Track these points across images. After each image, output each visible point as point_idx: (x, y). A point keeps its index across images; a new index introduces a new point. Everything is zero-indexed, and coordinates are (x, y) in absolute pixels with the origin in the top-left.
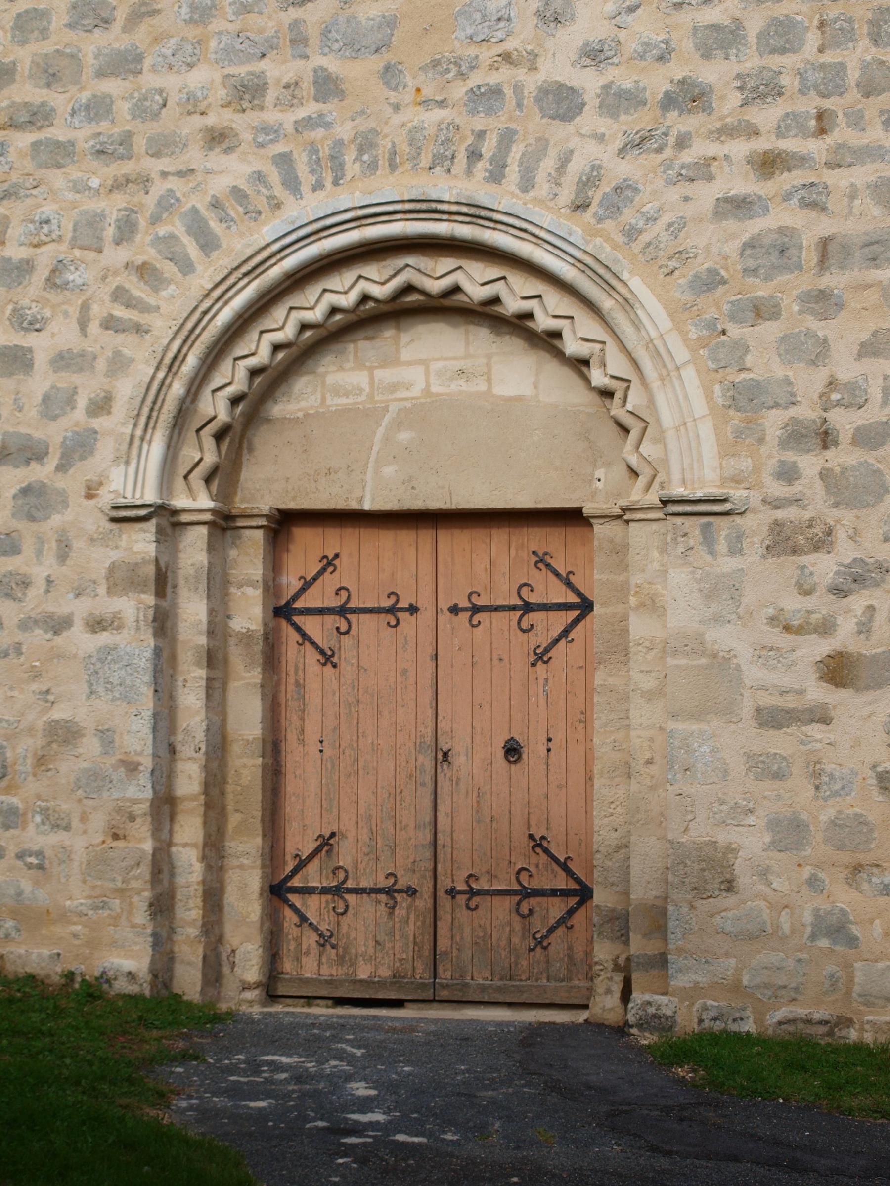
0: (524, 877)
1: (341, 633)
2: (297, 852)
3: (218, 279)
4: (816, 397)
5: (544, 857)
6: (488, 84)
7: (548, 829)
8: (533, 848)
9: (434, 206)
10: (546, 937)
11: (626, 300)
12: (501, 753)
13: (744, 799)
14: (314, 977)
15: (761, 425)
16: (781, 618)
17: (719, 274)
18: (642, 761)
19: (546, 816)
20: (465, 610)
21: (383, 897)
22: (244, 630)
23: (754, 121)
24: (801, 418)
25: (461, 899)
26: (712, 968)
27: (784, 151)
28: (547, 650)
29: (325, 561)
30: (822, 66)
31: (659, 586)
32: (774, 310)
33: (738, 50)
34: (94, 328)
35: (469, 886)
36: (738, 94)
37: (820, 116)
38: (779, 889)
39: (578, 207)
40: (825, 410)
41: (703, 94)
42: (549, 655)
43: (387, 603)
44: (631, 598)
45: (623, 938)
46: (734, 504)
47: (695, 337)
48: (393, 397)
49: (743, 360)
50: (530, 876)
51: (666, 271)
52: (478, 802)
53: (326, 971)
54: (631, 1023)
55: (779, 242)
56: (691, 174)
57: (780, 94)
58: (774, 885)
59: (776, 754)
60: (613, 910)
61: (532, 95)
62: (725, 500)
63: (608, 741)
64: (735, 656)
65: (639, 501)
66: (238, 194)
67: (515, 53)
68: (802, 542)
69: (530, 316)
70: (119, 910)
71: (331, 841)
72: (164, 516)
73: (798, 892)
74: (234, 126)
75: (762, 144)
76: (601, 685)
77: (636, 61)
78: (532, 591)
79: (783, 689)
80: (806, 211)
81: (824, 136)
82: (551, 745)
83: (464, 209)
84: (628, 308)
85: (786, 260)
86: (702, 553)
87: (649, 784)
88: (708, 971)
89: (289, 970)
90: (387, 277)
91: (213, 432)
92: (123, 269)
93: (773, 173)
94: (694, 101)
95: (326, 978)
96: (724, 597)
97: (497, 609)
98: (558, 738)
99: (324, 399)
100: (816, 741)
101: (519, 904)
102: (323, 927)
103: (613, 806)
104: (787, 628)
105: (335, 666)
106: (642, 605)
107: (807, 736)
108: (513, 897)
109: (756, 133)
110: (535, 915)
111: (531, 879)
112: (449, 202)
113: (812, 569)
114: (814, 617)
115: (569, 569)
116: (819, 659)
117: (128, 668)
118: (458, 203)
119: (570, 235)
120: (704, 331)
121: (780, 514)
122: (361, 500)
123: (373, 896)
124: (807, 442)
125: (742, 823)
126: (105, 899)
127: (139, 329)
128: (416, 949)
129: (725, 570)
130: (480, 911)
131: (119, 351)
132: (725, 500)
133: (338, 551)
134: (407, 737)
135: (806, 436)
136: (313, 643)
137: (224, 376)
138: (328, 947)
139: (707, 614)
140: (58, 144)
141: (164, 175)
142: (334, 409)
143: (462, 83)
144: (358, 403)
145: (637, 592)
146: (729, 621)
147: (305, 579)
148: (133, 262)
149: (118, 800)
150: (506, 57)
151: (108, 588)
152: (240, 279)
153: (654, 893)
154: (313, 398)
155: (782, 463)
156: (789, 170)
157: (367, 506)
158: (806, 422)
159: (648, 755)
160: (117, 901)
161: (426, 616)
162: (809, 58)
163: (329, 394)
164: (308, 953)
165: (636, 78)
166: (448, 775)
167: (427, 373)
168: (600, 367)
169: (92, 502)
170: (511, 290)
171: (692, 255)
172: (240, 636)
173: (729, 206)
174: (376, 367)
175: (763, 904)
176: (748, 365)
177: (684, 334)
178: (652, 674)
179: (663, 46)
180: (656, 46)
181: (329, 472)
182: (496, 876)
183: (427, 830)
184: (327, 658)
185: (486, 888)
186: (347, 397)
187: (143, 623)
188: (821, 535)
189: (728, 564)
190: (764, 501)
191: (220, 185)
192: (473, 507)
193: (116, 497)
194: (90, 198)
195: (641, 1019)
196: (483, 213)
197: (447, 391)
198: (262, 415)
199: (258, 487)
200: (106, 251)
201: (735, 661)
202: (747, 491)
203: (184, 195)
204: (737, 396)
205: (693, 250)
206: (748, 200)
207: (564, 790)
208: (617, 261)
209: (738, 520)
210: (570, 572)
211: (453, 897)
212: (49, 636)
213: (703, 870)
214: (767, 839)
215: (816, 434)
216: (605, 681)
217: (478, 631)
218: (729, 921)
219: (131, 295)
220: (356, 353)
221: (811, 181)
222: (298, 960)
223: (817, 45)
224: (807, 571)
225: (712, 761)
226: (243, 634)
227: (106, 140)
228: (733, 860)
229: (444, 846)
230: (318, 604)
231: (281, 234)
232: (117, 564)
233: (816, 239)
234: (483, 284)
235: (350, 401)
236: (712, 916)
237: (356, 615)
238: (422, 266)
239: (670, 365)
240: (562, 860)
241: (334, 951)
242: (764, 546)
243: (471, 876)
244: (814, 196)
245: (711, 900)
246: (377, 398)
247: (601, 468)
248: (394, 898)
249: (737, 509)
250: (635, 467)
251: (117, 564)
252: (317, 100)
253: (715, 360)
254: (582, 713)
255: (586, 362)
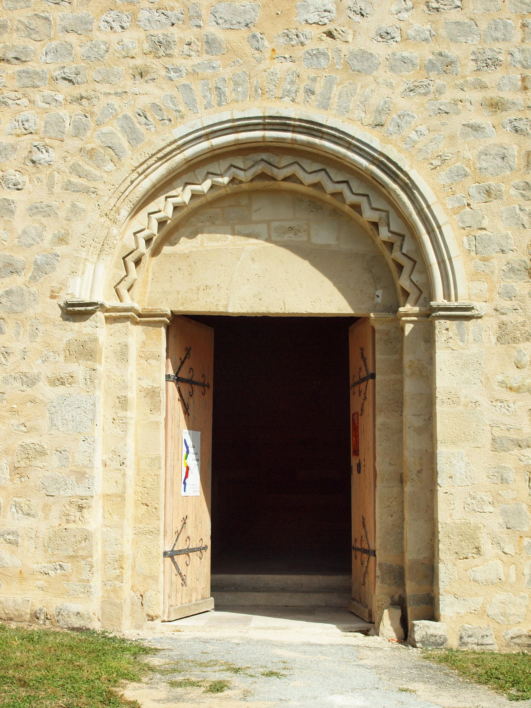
3: (142, 160)
22: (150, 387)
33: (473, 38)
34: (57, 189)
36: (473, 63)
70: (70, 571)
91: (134, 259)
94: (447, 66)
119: (372, 142)
122: (226, 306)
153: (423, 555)
160: (70, 565)
167: (269, 228)
177: (444, 205)
180: (423, 33)
191: (143, 102)
195: (423, 637)
238: (272, 160)
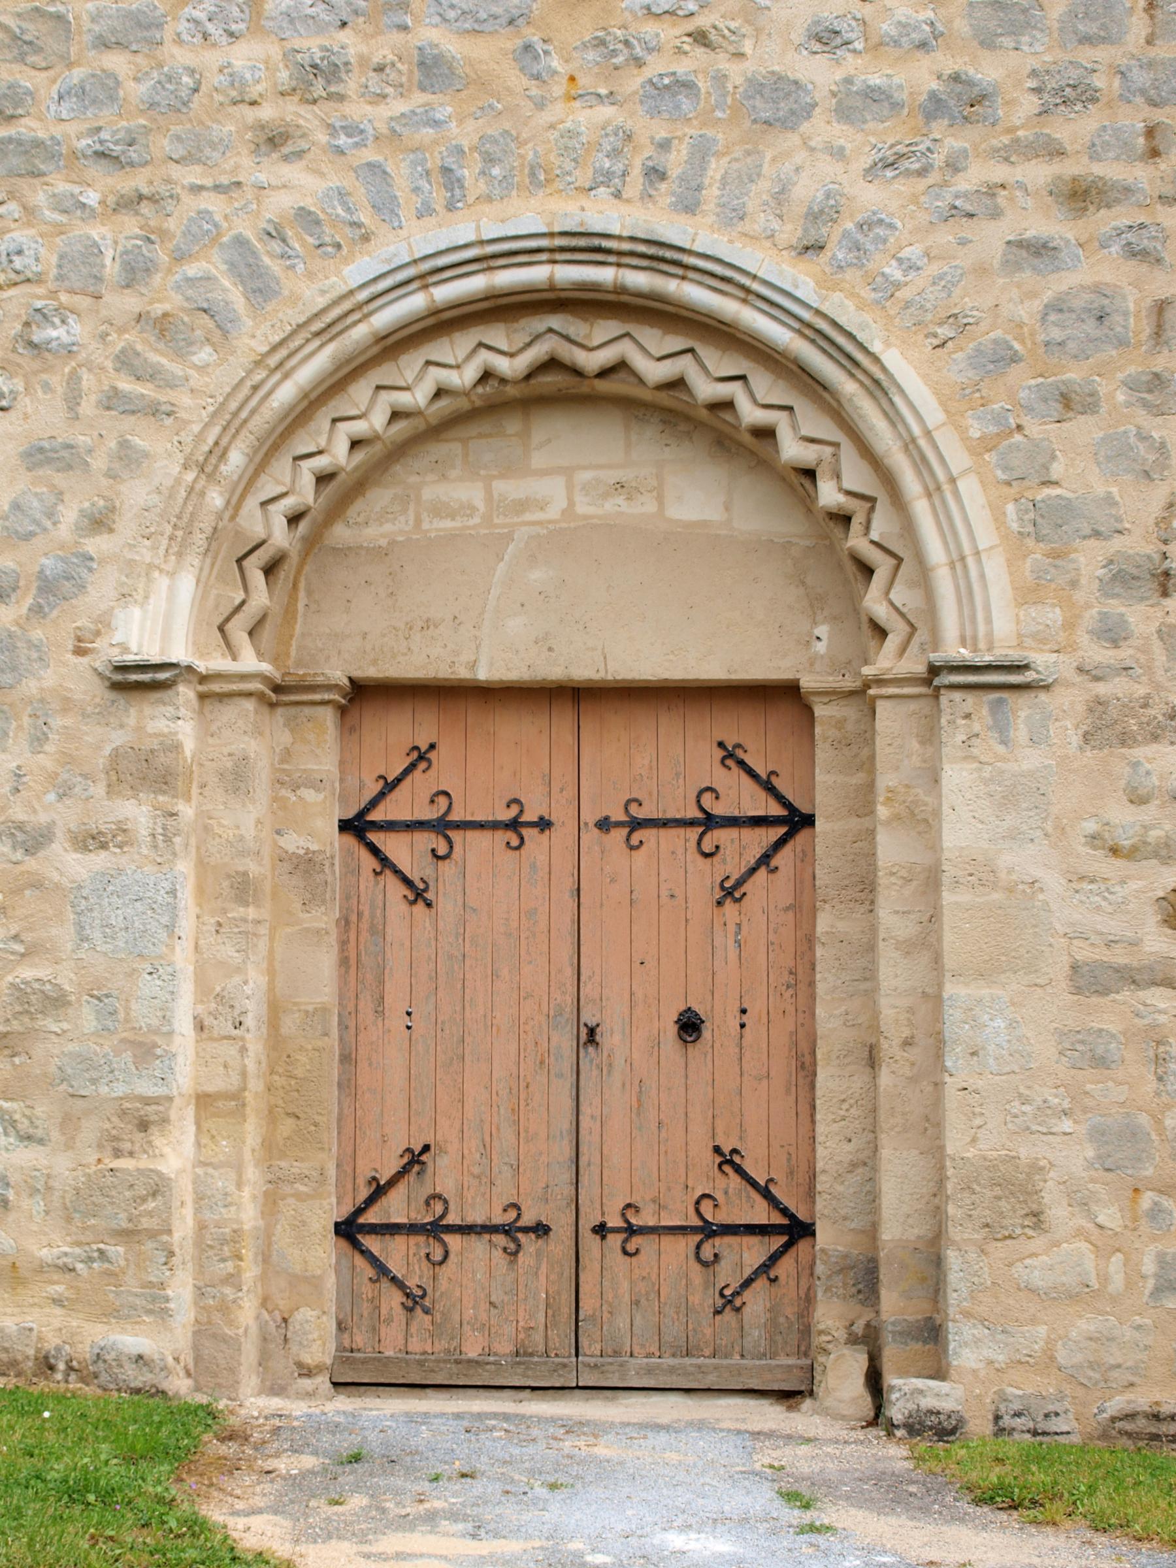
0: (706, 1208)
1: (438, 858)
2: (373, 1174)
4: (1151, 521)
5: (735, 1180)
6: (674, 74)
7: (741, 1138)
8: (720, 1166)
9: (596, 242)
10: (738, 1293)
11: (877, 382)
12: (672, 1030)
13: (1056, 1096)
14: (400, 1355)
15: (1073, 561)
16: (1107, 835)
17: (1011, 348)
18: (896, 1042)
19: (738, 1121)
20: (619, 824)
21: (500, 1240)
22: (302, 852)
23: (1058, 136)
24: (1131, 552)
25: (615, 1240)
26: (1012, 1340)
27: (1101, 178)
28: (740, 883)
29: (415, 755)
30: (1151, 65)
31: (919, 790)
32: (1089, 400)
34: (87, 408)
35: (627, 1221)
36: (1034, 98)
37: (1150, 132)
38: (1107, 1224)
39: (807, 248)
40: (1165, 542)
41: (984, 97)
42: (743, 890)
43: (507, 815)
44: (879, 807)
45: (860, 1296)
46: (1038, 672)
47: (977, 435)
48: (520, 520)
49: (1048, 469)
50: (716, 1206)
51: (936, 342)
52: (639, 1100)
53: (415, 1345)
54: (896, 1422)
55: (1096, 305)
56: (969, 208)
57: (1094, 100)
58: (1101, 1219)
59: (1101, 1030)
60: (846, 1256)
61: (737, 91)
62: (1026, 667)
63: (836, 1012)
64: (1042, 890)
65: (892, 668)
66: (306, 218)
67: (713, 30)
68: (1135, 728)
69: (728, 405)
71: (424, 1158)
72: (190, 682)
73: (1135, 1229)
74: (301, 122)
75: (1071, 168)
76: (827, 933)
77: (887, 48)
78: (717, 798)
79: (1111, 938)
80: (1133, 262)
81: (1158, 160)
82: (745, 1018)
83: (642, 248)
84: (878, 393)
85: (1107, 331)
86: (992, 742)
87: (909, 1074)
88: (1007, 1345)
89: (361, 1345)
90: (521, 345)
91: (262, 563)
92: (133, 323)
93: (1085, 209)
94: (972, 106)
95: (417, 1357)
96: (1024, 805)
97: (665, 823)
98: (756, 1008)
99: (418, 522)
100: (1160, 1012)
101: (698, 1247)
102: (412, 1282)
103: (845, 1106)
104: (1115, 851)
105: (429, 905)
106: (897, 817)
107: (1146, 1005)
108: (773, 1239)
109: (1061, 153)
110: (723, 1263)
111: (717, 1210)
112: (619, 238)
113: (1148, 766)
114: (1154, 835)
115: (770, 769)
116: (1161, 894)
117: (138, 904)
118: (633, 239)
119: (797, 287)
120: (991, 428)
121: (1101, 689)
122: (473, 665)
123: (487, 1237)
124: (1140, 587)
125: (1054, 1130)
126: (102, 1246)
127: (154, 411)
128: (550, 1312)
129: (1026, 766)
130: (642, 1257)
131: (127, 441)
132: (1026, 667)
133: (433, 741)
134: (536, 1008)
135: (1138, 578)
136: (397, 872)
137: (279, 482)
138: (418, 1310)
139: (1000, 830)
140: (38, 144)
141: (197, 189)
142: (433, 535)
143: (635, 72)
144: (469, 528)
145: (888, 799)
146: (1032, 840)
147: (385, 779)
148: (148, 312)
149: (121, 1098)
150: (700, 38)
151: (109, 786)
152: (308, 341)
153: (916, 1231)
154: (402, 519)
155: (1104, 616)
156: (1108, 206)
157: (483, 674)
158: (1138, 558)
159: (906, 1033)
161: (563, 834)
162: (1135, 51)
163: (425, 514)
164: (389, 1320)
165: (889, 72)
166: (597, 1061)
167: (570, 488)
168: (832, 479)
169: (85, 660)
170: (703, 367)
171: (971, 320)
172: (295, 861)
173: (1024, 253)
174: (494, 477)
175: (1084, 1246)
176: (1054, 477)
177: (962, 431)
178: (912, 917)
179: (927, 28)
180: (916, 28)
181: (428, 624)
182: (665, 1207)
183: (566, 1142)
184: (418, 894)
185: (651, 1224)
186: (453, 519)
187: (161, 837)
188: (1161, 718)
189: (1030, 760)
190: (1080, 670)
191: (280, 204)
192: (637, 677)
193: (122, 654)
194: (83, 220)
195: (910, 1416)
196: (669, 254)
197: (600, 512)
198: (327, 542)
199: (320, 645)
200: (108, 298)
201: (1041, 897)
202: (1056, 655)
203: (226, 217)
204: (1039, 520)
205: (975, 313)
206: (1051, 245)
207: (765, 1082)
208: (863, 326)
209: (1043, 696)
210: (773, 773)
211: (603, 1238)
212: (19, 855)
213: (999, 1198)
214: (1090, 1153)
215: (1153, 575)
216: (832, 927)
217: (640, 856)
218: (1036, 1273)
219: (146, 360)
220: (466, 455)
221: (1139, 222)
222: (374, 1330)
223: (1144, 34)
224: (1142, 771)
225: (1009, 1041)
226: (298, 856)
227: (108, 137)
228: (1041, 1184)
229: (589, 1165)
230: (405, 816)
231: (372, 277)
232: (121, 750)
233: (1149, 302)
234: (660, 359)
235: (457, 524)
236: (1010, 1265)
237: (462, 832)
239: (941, 475)
240: (762, 1183)
241: (428, 1318)
242: (1080, 732)
243: (629, 1206)
244: (1146, 241)
245: (1009, 1242)
246: (496, 521)
247: (823, 623)
248: (515, 1240)
249: (1042, 680)
250: (882, 623)
251: (121, 750)
252: (423, 89)
253: (1006, 468)
254: (791, 973)
255: (810, 474)
